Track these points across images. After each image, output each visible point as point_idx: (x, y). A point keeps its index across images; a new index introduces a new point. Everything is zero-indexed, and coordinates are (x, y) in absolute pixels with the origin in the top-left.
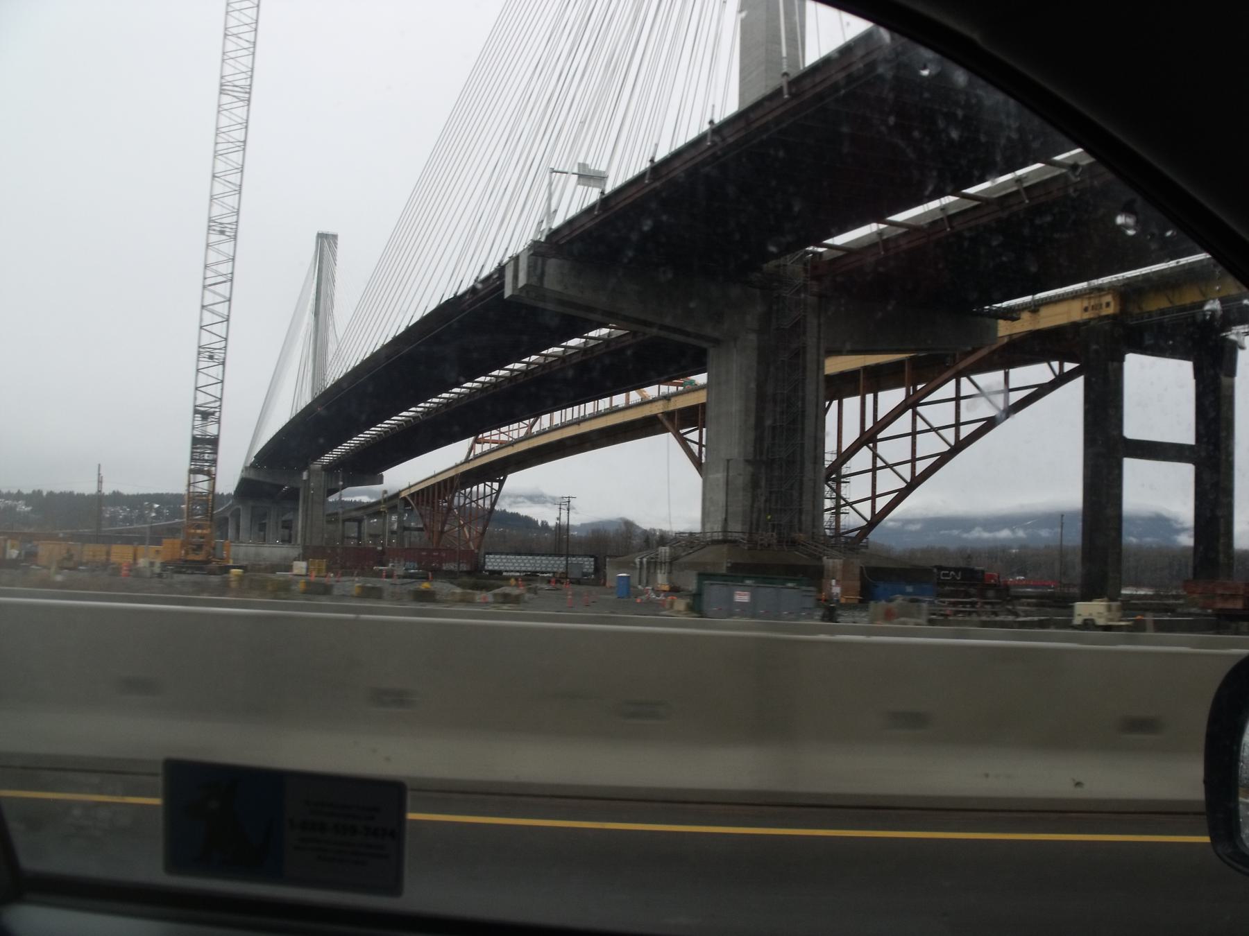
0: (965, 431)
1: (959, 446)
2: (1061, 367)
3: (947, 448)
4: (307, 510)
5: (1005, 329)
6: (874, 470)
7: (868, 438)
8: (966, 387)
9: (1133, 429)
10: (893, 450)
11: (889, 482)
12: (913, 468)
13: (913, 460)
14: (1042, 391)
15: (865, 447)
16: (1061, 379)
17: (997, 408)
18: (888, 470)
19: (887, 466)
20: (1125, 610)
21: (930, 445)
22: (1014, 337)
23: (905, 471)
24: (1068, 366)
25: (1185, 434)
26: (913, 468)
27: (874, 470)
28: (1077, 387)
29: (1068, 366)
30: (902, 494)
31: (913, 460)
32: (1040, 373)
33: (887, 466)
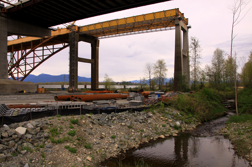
0: (45, 57)
1: (43, 60)
2: (65, 44)
3: (51, 54)
4: (4, 94)
5: (53, 34)
6: (34, 57)
7: (23, 57)
8: (45, 48)
9: (80, 55)
10: (29, 61)
11: (29, 68)
12: (34, 65)
13: (43, 56)
14: (61, 49)
15: (22, 60)
16: (65, 47)
17: (41, 60)
18: (38, 56)
19: (28, 64)
20: (150, 82)
21: (37, 60)
22: (55, 36)
23: (32, 65)
24: (66, 44)
25: (89, 57)
26: (34, 65)
27: (34, 57)
28: (68, 49)
29: (66, 44)
30: (32, 70)
31: (34, 63)
32: (61, 46)
33: (28, 64)
